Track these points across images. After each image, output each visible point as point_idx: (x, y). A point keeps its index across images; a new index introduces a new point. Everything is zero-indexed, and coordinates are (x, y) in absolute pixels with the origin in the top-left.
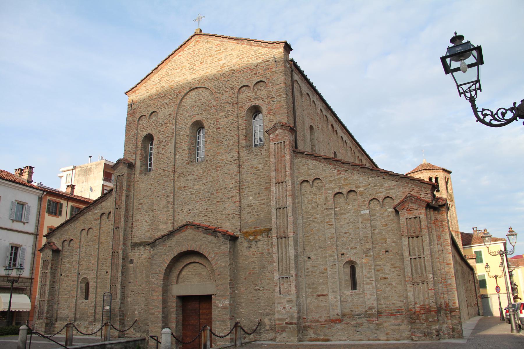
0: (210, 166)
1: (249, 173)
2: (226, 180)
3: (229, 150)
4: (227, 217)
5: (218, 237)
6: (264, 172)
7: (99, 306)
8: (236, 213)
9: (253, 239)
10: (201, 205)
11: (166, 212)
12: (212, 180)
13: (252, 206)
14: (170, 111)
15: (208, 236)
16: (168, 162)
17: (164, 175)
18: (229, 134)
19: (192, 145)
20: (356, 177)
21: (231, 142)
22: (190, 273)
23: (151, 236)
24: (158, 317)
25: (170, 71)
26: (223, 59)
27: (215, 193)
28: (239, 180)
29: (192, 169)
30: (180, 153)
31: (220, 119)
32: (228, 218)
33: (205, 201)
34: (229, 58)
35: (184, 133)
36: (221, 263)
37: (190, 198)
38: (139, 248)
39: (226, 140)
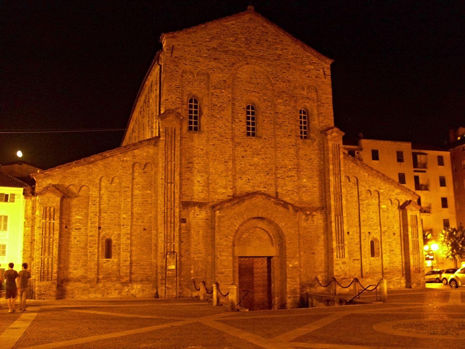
7: (135, 266)
9: (310, 214)
13: (306, 187)
24: (229, 276)
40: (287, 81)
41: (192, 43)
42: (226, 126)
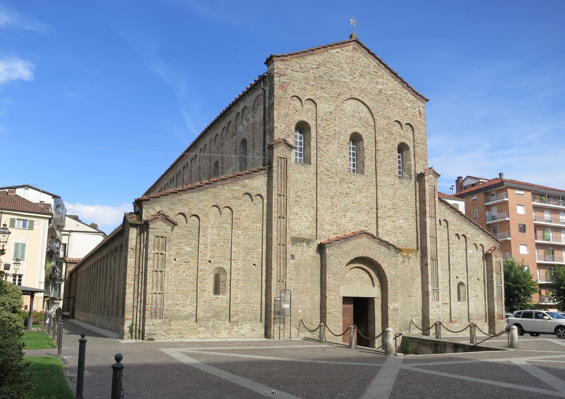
0: (369, 181)
1: (401, 199)
2: (385, 200)
4: (386, 233)
5: (390, 249)
6: (411, 203)
9: (406, 256)
10: (362, 215)
11: (331, 213)
13: (403, 228)
14: (330, 109)
17: (328, 175)
18: (387, 160)
20: (466, 226)
22: (353, 277)
29: (354, 179)
30: (341, 158)
31: (379, 141)
36: (393, 272)
37: (352, 207)
38: (301, 244)
39: (385, 164)
40: (387, 118)
41: (299, 68)
42: (332, 161)
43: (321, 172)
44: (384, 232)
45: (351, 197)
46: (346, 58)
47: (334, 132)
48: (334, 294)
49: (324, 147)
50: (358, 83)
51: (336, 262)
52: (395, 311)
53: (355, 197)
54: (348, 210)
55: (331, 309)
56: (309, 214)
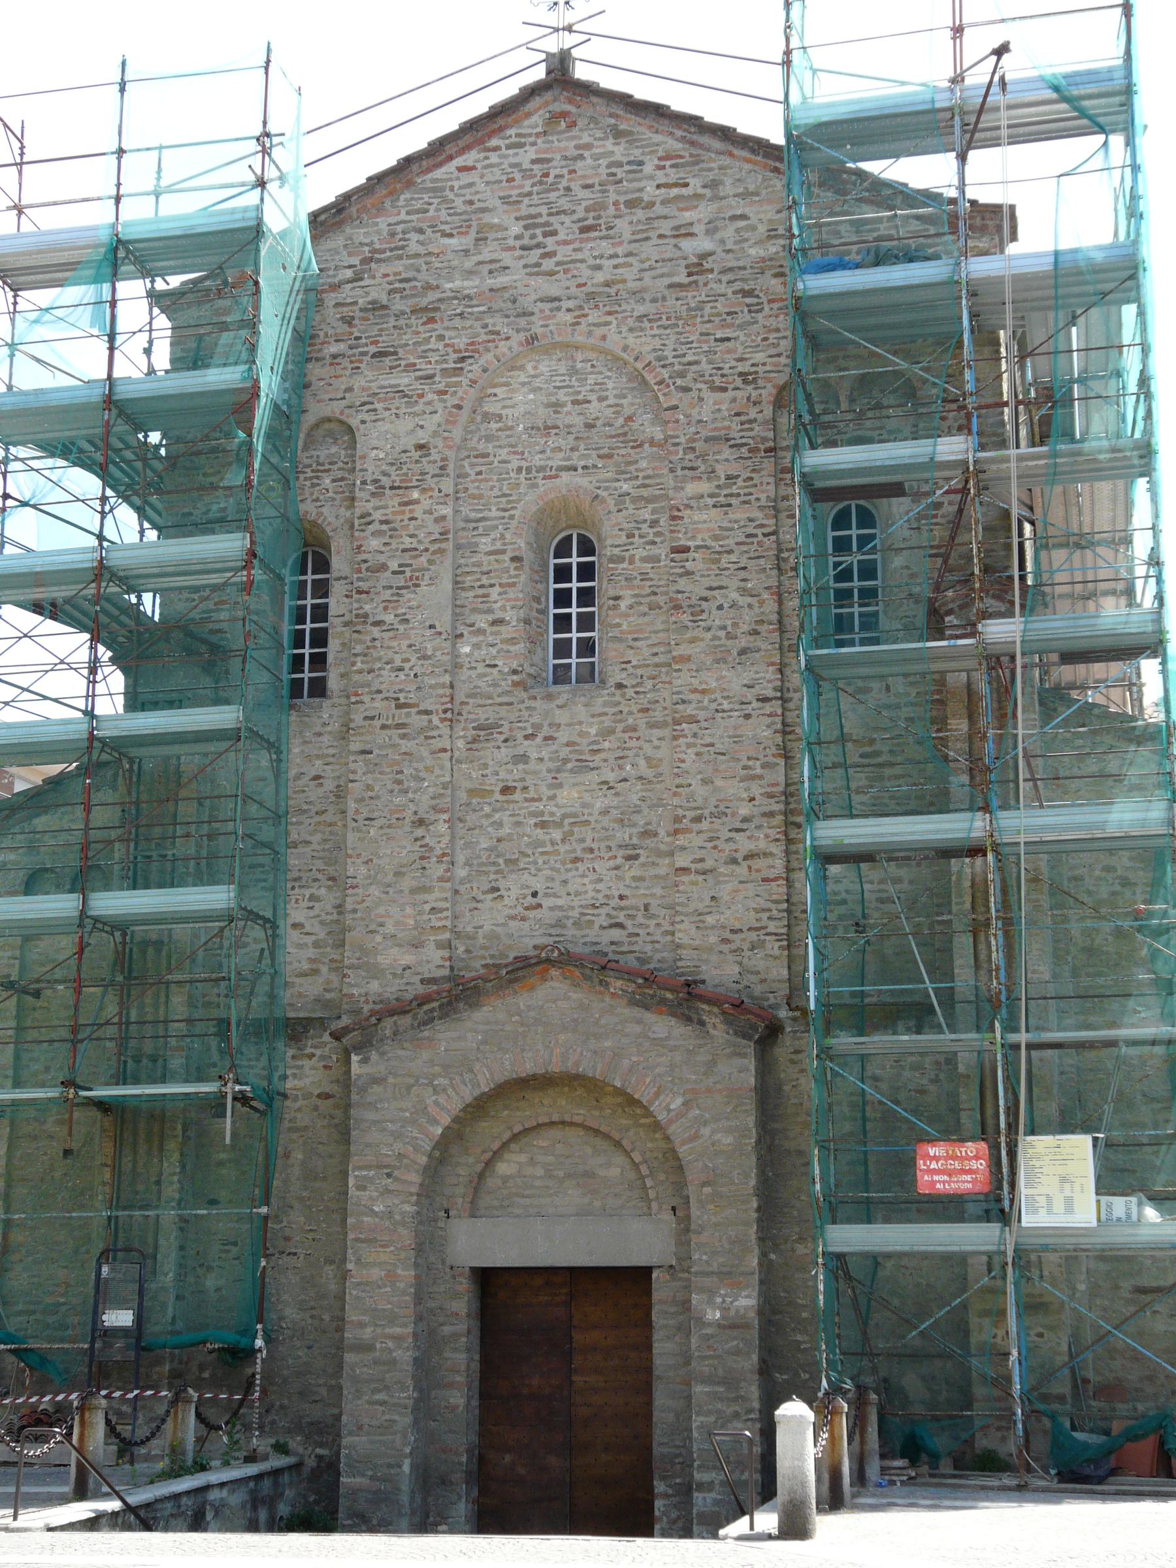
0: (634, 709)
3: (735, 653)
4: (725, 941)
8: (772, 927)
11: (413, 891)
12: (649, 773)
13: (844, 902)
14: (420, 433)
15: (649, 1017)
16: (417, 669)
19: (535, 605)
21: (747, 620)
23: (328, 996)
25: (414, 237)
26: (698, 229)
27: (662, 832)
28: (781, 788)
30: (481, 632)
31: (688, 506)
32: (733, 946)
33: (612, 863)
34: (729, 232)
35: (498, 545)
37: (539, 843)
43: (366, 718)
44: (713, 939)
45: (526, 800)
46: (509, 180)
47: (436, 529)
48: (383, 1258)
49: (385, 608)
50: (566, 271)
51: (401, 1110)
52: (735, 1332)
53: (553, 798)
54: (515, 862)
55: (369, 1330)
56: (312, 913)
